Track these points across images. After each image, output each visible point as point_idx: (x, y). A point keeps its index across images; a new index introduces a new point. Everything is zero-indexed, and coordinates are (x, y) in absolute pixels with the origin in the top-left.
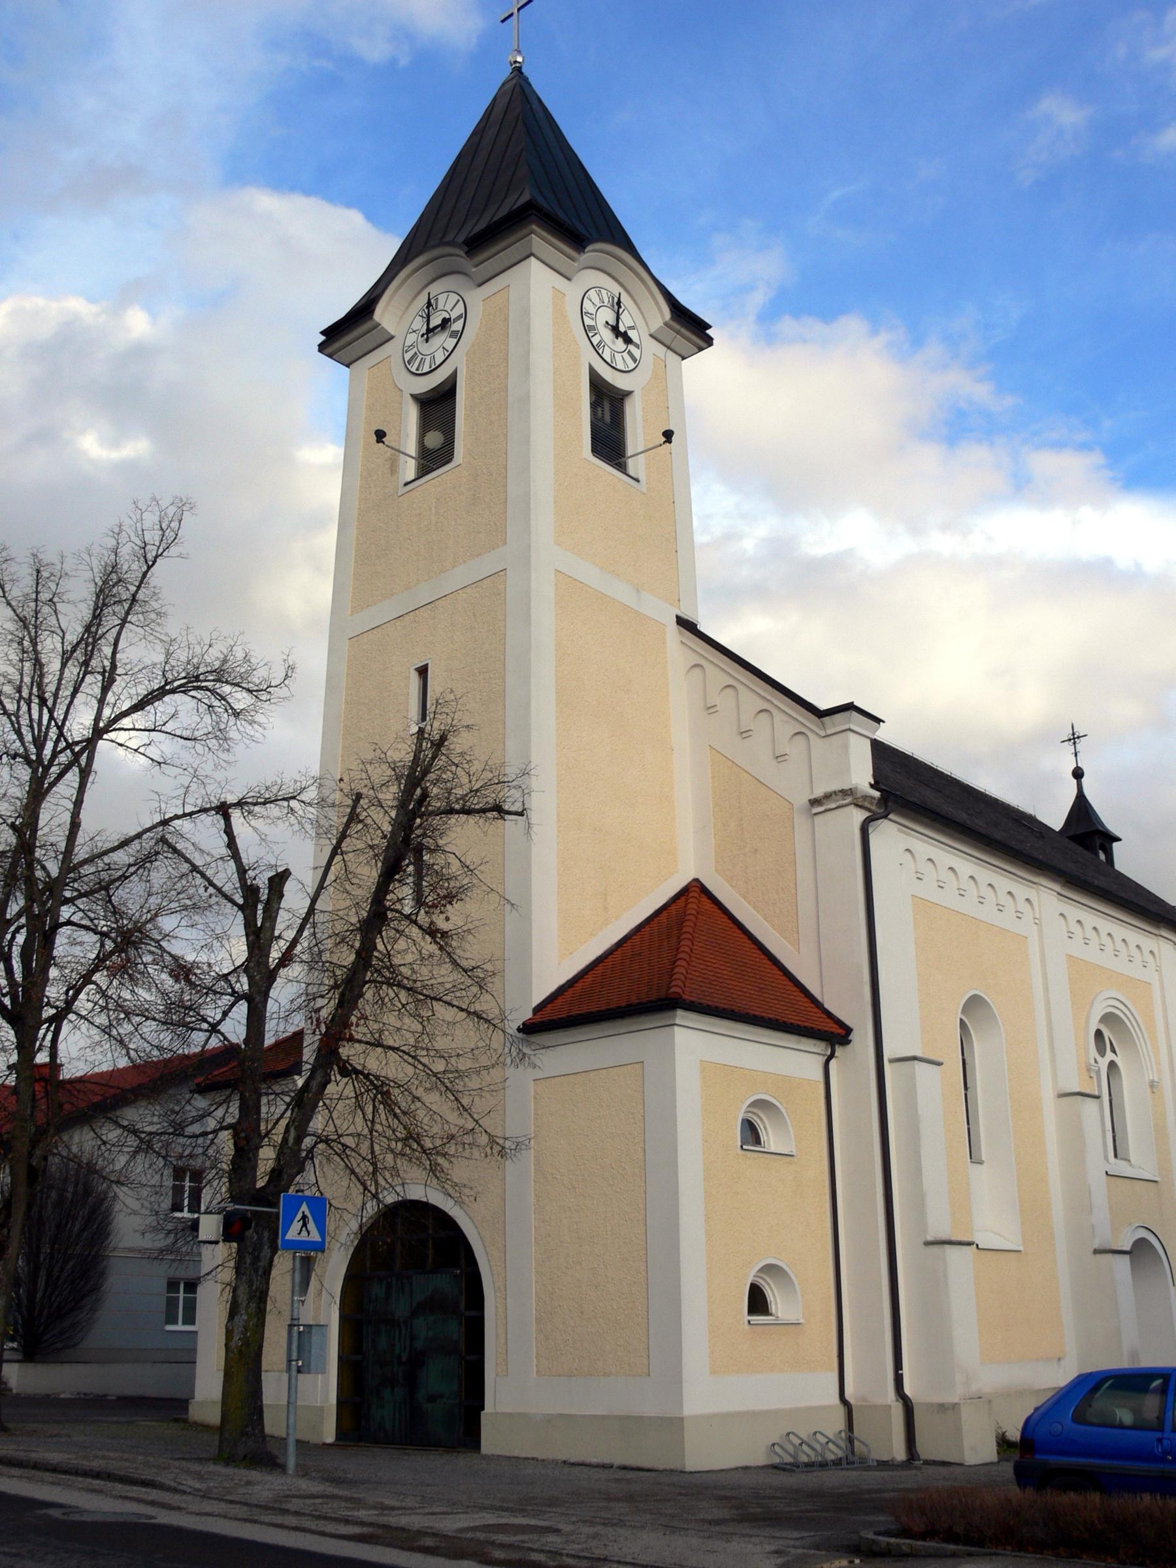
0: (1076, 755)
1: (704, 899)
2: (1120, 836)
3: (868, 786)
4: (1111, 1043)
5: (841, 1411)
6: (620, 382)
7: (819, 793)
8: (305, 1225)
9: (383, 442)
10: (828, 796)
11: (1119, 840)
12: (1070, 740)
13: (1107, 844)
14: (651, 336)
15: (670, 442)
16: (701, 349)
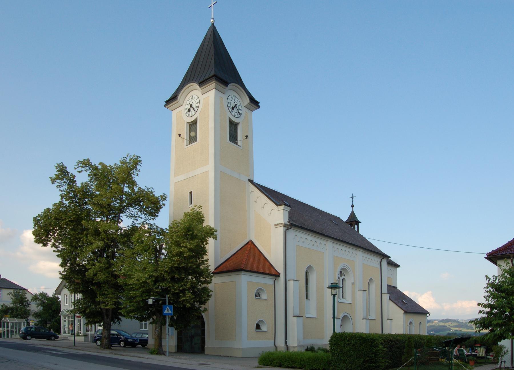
1: (252, 245)
3: (287, 222)
5: (275, 348)
6: (236, 120)
7: (276, 223)
8: (168, 310)
10: (278, 224)
11: (361, 222)
13: (357, 223)
14: (245, 107)
15: (247, 138)
16: (257, 109)
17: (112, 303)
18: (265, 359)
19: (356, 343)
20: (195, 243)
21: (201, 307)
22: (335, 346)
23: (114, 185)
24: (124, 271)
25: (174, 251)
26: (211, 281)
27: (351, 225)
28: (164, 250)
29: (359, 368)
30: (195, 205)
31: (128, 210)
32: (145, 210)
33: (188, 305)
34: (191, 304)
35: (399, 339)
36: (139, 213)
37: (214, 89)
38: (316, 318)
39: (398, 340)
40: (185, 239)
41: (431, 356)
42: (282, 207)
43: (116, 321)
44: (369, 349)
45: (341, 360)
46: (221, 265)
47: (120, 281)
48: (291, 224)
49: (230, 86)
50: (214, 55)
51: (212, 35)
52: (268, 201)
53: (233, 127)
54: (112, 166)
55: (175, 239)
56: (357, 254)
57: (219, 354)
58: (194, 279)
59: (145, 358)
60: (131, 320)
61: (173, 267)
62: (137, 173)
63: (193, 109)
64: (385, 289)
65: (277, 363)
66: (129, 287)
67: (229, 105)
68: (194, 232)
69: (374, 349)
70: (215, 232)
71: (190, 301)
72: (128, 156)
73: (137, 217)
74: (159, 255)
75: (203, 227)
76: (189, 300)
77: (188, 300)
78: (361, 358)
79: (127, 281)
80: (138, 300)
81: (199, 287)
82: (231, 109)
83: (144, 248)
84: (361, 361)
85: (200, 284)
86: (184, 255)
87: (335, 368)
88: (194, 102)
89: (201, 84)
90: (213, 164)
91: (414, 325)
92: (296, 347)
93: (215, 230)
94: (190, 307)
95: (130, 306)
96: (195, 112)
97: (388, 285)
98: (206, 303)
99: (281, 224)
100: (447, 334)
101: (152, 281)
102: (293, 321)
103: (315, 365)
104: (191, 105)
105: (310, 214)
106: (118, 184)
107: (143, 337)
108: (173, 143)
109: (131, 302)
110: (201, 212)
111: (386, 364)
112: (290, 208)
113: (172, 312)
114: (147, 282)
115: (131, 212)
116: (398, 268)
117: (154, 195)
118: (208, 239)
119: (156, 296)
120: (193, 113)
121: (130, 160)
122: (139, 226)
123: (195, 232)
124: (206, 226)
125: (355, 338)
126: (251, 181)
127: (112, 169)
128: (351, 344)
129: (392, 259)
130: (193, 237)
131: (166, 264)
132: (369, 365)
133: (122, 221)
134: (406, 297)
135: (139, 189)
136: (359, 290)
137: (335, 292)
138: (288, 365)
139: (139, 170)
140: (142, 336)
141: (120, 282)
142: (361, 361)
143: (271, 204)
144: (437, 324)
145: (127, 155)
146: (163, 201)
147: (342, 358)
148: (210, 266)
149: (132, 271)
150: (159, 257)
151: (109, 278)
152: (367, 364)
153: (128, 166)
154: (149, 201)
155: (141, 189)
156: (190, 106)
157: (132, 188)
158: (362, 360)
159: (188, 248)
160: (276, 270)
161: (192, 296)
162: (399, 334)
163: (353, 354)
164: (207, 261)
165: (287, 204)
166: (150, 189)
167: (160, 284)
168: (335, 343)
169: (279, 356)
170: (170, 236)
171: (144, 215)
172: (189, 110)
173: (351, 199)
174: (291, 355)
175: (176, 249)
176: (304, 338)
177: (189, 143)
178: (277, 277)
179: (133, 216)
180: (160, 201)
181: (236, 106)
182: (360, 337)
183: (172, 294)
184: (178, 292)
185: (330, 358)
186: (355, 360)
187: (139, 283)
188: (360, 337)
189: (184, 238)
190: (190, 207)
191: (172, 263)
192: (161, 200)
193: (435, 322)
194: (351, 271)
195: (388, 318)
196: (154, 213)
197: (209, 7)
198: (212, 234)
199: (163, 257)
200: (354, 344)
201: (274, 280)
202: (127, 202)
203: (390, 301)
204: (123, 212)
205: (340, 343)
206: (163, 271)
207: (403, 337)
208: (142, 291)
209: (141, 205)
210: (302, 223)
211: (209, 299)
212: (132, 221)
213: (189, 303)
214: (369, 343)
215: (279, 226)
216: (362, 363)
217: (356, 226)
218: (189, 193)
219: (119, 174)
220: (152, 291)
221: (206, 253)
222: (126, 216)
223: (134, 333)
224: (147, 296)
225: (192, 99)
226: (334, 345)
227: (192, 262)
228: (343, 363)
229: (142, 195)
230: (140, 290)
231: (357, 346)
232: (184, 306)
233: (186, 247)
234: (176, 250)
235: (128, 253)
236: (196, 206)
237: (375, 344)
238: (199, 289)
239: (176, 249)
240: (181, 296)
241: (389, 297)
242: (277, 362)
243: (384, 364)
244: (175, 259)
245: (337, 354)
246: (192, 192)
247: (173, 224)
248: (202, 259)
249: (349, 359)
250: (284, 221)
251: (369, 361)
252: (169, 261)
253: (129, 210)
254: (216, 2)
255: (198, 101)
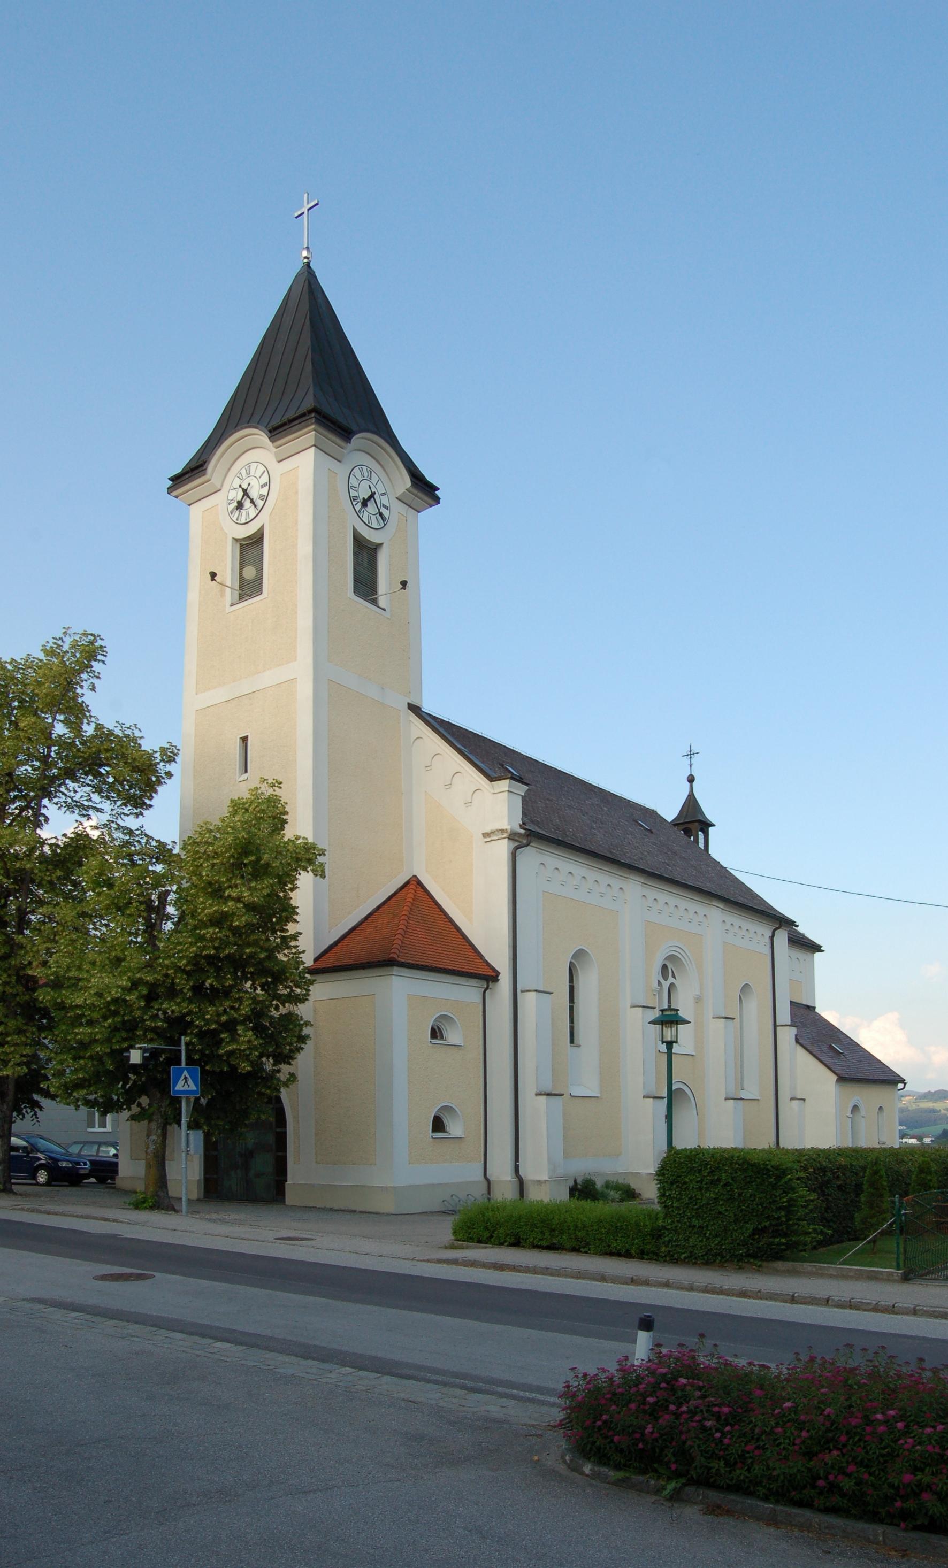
0: (691, 766)
2: (714, 822)
3: (519, 827)
4: (673, 972)
5: (486, 1184)
7: (488, 830)
9: (215, 580)
10: (493, 832)
11: (714, 825)
12: (693, 754)
14: (397, 498)
15: (405, 589)
16: (431, 506)
17: (17, 1059)
18: (474, 1225)
19: (733, 1179)
20: (263, 888)
21: (279, 1071)
22: (675, 1186)
23: (23, 715)
24: (57, 967)
25: (203, 909)
26: (308, 995)
27: (688, 832)
28: (173, 906)
29: (740, 1249)
30: (261, 778)
31: (63, 789)
32: (111, 786)
33: (245, 1067)
34: (252, 1062)
35: (843, 1163)
36: (96, 797)
37: (313, 448)
38: (597, 1097)
39: (840, 1167)
40: (234, 876)
41: (941, 1217)
42: (504, 785)
43: (27, 1112)
44: (771, 1197)
45: (690, 1226)
46: (331, 947)
47: (44, 996)
48: (528, 833)
49: (357, 440)
50: (312, 350)
51: (306, 297)
52: (464, 766)
53: (365, 554)
54: (19, 661)
55: (207, 875)
56: (708, 916)
57: (328, 1206)
58: (259, 991)
59: (122, 1222)
60: (76, 1109)
61: (200, 955)
62: (93, 684)
63: (252, 501)
64: (784, 1015)
65: (507, 1235)
66: (72, 1014)
67: (353, 493)
68: (260, 857)
69: (784, 1197)
70: (318, 857)
71: (250, 1054)
72: (65, 633)
73: (89, 807)
74: (158, 922)
75: (286, 839)
76: (247, 1052)
77: (244, 1050)
78: (747, 1223)
79: (66, 997)
80: (97, 1052)
81: (274, 1013)
82: (360, 504)
83: (116, 900)
84: (747, 1229)
85: (277, 1005)
86: (232, 921)
87: (674, 1249)
88: (254, 482)
89: (276, 431)
90: (309, 660)
91: (863, 1113)
92: (546, 1181)
93: (318, 850)
94: (249, 1072)
95: (72, 1070)
96: (257, 512)
97: (791, 1001)
98: (293, 1059)
99: (502, 831)
100: (941, 1132)
101: (140, 997)
102: (533, 1106)
103: (616, 1240)
104: (245, 493)
105: (578, 803)
106: (35, 714)
107: (100, 1154)
108: (193, 596)
109: (75, 1058)
110: (281, 797)
111: (815, 1238)
112: (527, 788)
113: (196, 1086)
114: (127, 1001)
115: (72, 794)
116: (817, 955)
117: (140, 745)
118: (300, 874)
119: (151, 1040)
120: (253, 512)
121: (72, 647)
122: (95, 834)
123: (266, 856)
124: (293, 839)
125: (731, 1164)
126: (415, 709)
127: (18, 671)
128: (720, 1182)
129: (801, 929)
130: (260, 871)
131: (179, 948)
132: (771, 1240)
133: (47, 820)
134: (840, 1035)
135: (96, 729)
136: (713, 1018)
137: (671, 1033)
138: (540, 1240)
139: (96, 674)
140: (98, 1151)
141: (44, 998)
142: (747, 1229)
143: (470, 776)
144: (914, 1106)
145: (64, 630)
146: (168, 765)
147: (695, 1222)
148: (304, 952)
149: (79, 968)
150: (157, 927)
151: (12, 988)
152: (763, 1238)
153: (68, 663)
154: (126, 763)
155: (104, 728)
156: (242, 493)
157: (76, 727)
158: (750, 1227)
159: (244, 903)
160: (488, 964)
161: (255, 1040)
162: (840, 1149)
163: (726, 1210)
164: (296, 940)
165: (515, 773)
166: (129, 728)
167: (162, 1004)
168: (674, 1177)
169: (512, 1216)
170: (191, 868)
171: (109, 802)
172: (240, 506)
173: (686, 761)
174: (549, 1212)
175: (211, 905)
176: (566, 1156)
177: (240, 599)
178: (490, 983)
179: (78, 804)
180: (158, 763)
181: (372, 496)
182: (744, 1162)
183: (196, 1035)
184: (214, 1030)
185: (660, 1223)
186: (731, 1228)
187: (104, 1004)
188: (745, 1161)
189: (232, 872)
190: (240, 780)
191: (199, 944)
192: (161, 761)
193: (907, 1098)
194: (693, 964)
195: (792, 1097)
196: (141, 797)
197: (296, 215)
198: (310, 861)
199: (168, 926)
200: (728, 1182)
201: (483, 990)
202: (61, 765)
203: (799, 1049)
204: (50, 796)
205: (687, 1180)
206: (172, 968)
207: (853, 1156)
208: (110, 1026)
209: (101, 774)
210: (559, 829)
211: (302, 1049)
212: (77, 821)
213: (246, 1059)
214: (771, 1180)
215: (495, 838)
216: (749, 1236)
217: (701, 836)
218: (238, 740)
219: (40, 687)
220: (140, 1025)
221: (295, 917)
222: (57, 804)
223: (75, 1143)
224: (124, 1040)
225: (248, 473)
226: (672, 1184)
227: (255, 943)
228: (697, 1236)
229: (105, 747)
230: (106, 1025)
231: (737, 1188)
232: (234, 1068)
233: (238, 900)
234: (208, 908)
235: (66, 912)
236: (263, 782)
237: (786, 1183)
238: (272, 1017)
239: (211, 905)
240: (222, 1040)
241: (794, 1037)
242: (509, 1232)
243: (812, 1238)
244: (208, 933)
245: (678, 1208)
246: (247, 737)
247: (200, 833)
248: (283, 934)
249: (714, 1224)
250: (508, 824)
251: (771, 1231)
252: (190, 940)
253: (67, 789)
254: (316, 202)
255: (265, 479)
